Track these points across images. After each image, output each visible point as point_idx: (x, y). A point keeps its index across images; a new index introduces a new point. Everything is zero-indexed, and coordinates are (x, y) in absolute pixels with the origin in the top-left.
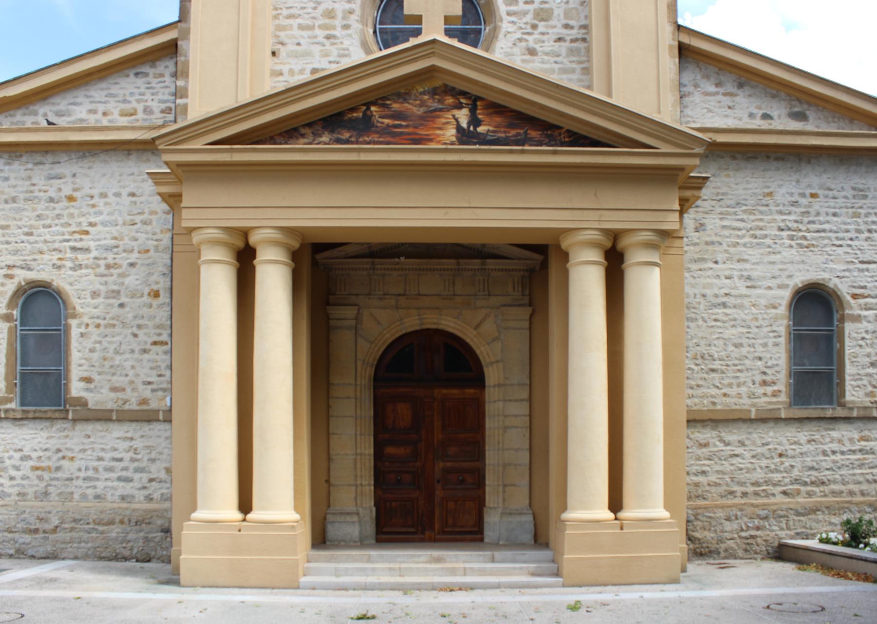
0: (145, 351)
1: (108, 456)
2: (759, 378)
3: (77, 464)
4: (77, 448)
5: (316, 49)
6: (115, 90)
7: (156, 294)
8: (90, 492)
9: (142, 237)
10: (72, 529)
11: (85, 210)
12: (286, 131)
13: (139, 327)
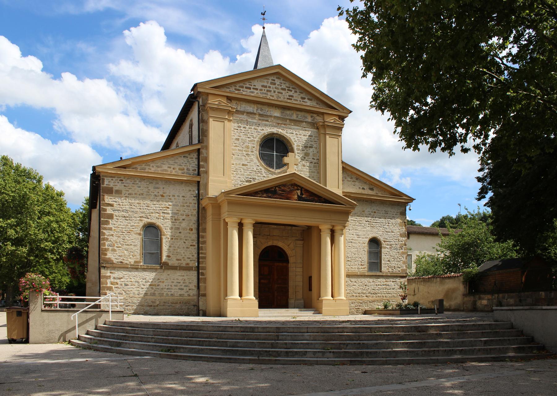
0: (187, 248)
1: (175, 281)
2: (360, 263)
3: (165, 284)
4: (165, 279)
5: (243, 158)
6: (177, 161)
7: (192, 230)
8: (169, 293)
9: (187, 211)
10: (164, 305)
11: (167, 200)
12: (254, 193)
13: (186, 240)
